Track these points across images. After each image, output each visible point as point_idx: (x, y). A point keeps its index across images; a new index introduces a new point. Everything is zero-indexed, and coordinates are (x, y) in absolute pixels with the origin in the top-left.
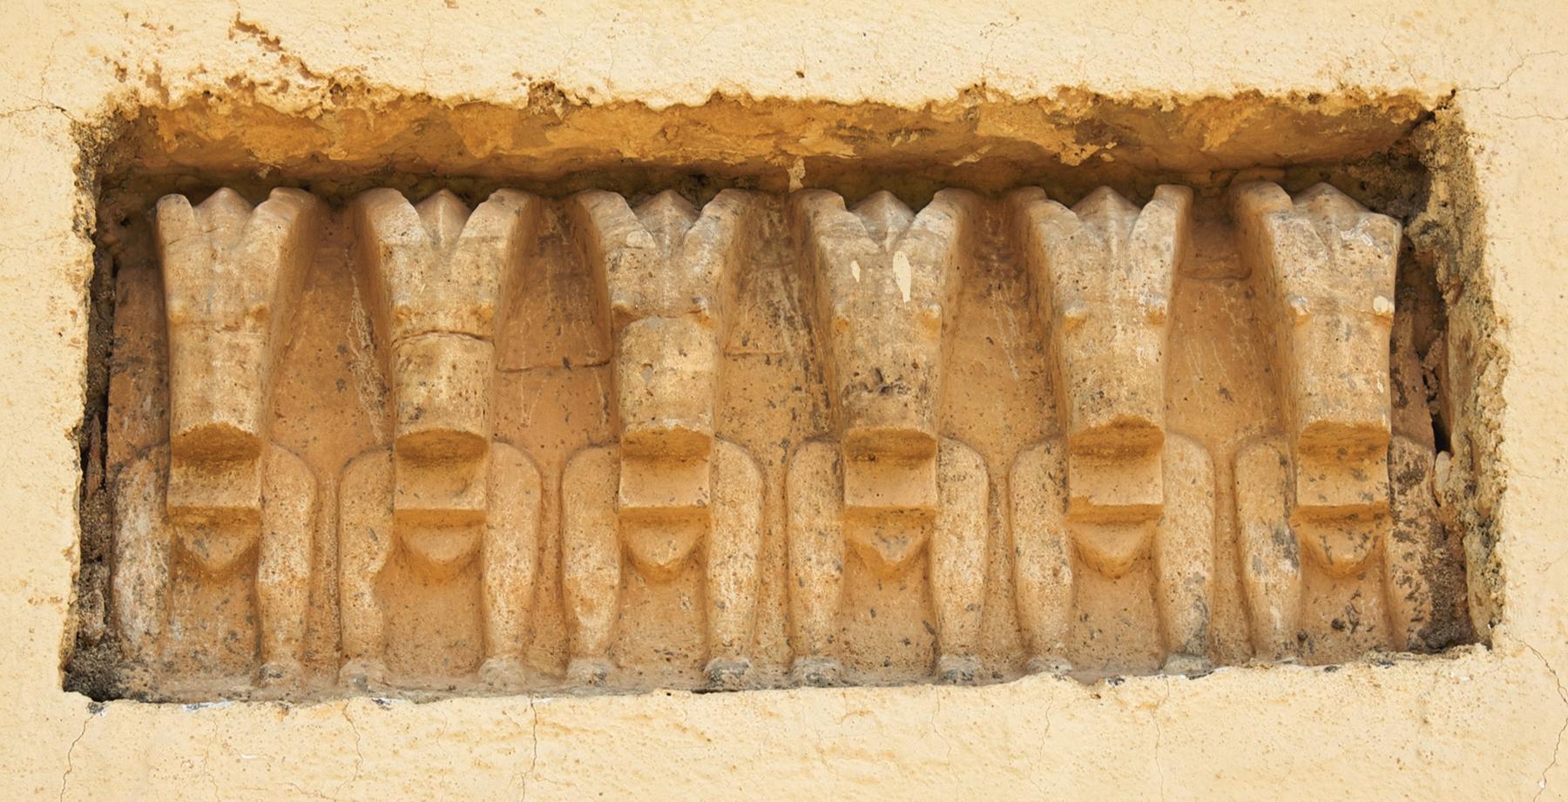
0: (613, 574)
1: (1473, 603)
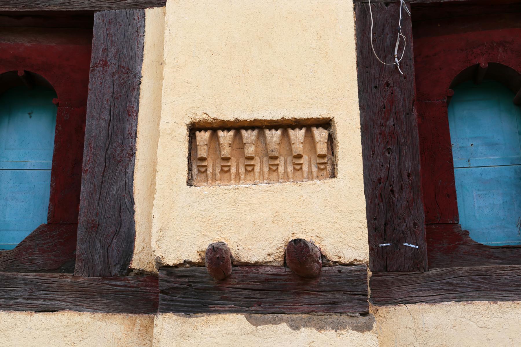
0: (244, 171)
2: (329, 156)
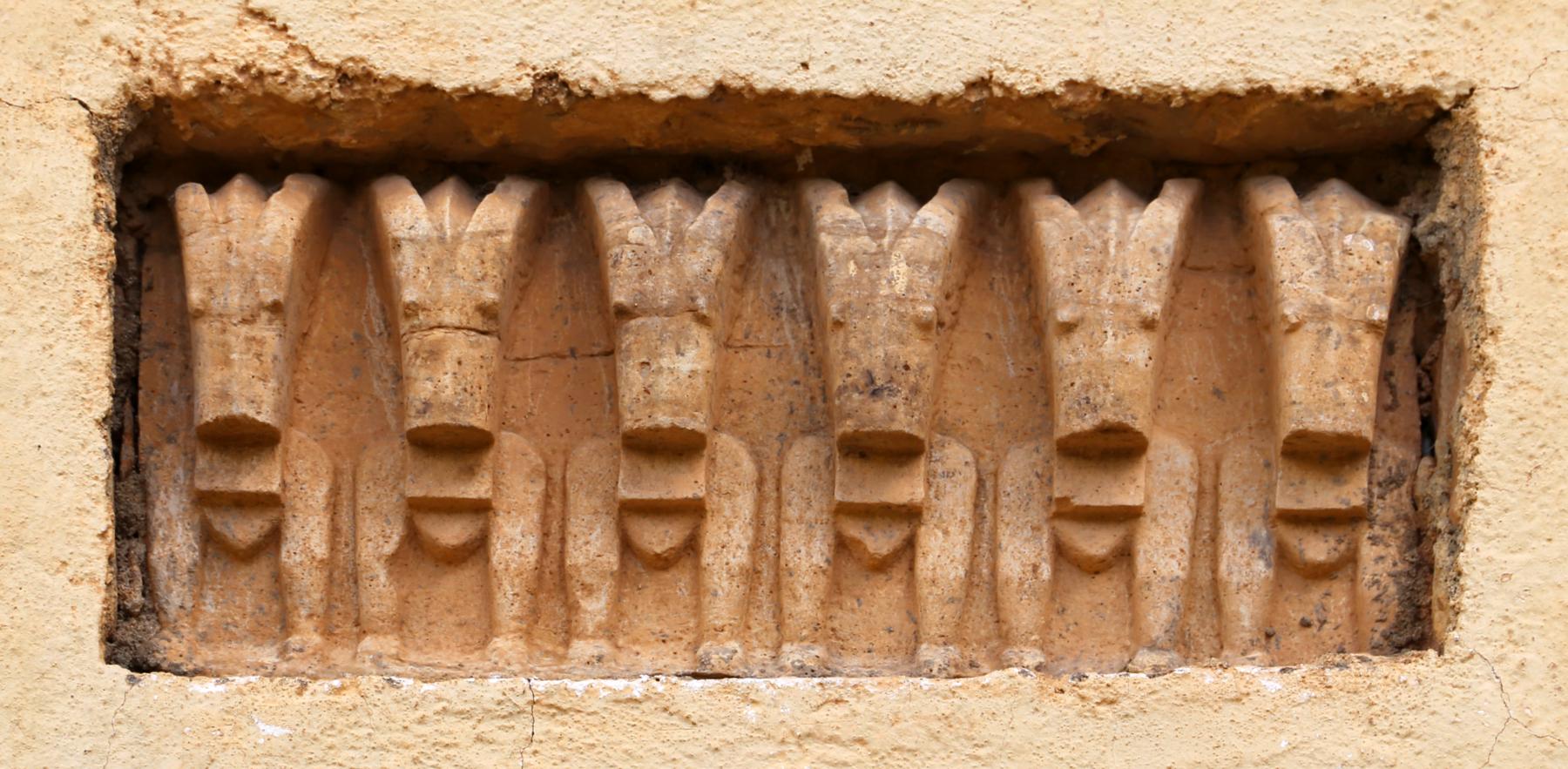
0: (612, 560)
1: (1435, 607)
2: (1392, 453)
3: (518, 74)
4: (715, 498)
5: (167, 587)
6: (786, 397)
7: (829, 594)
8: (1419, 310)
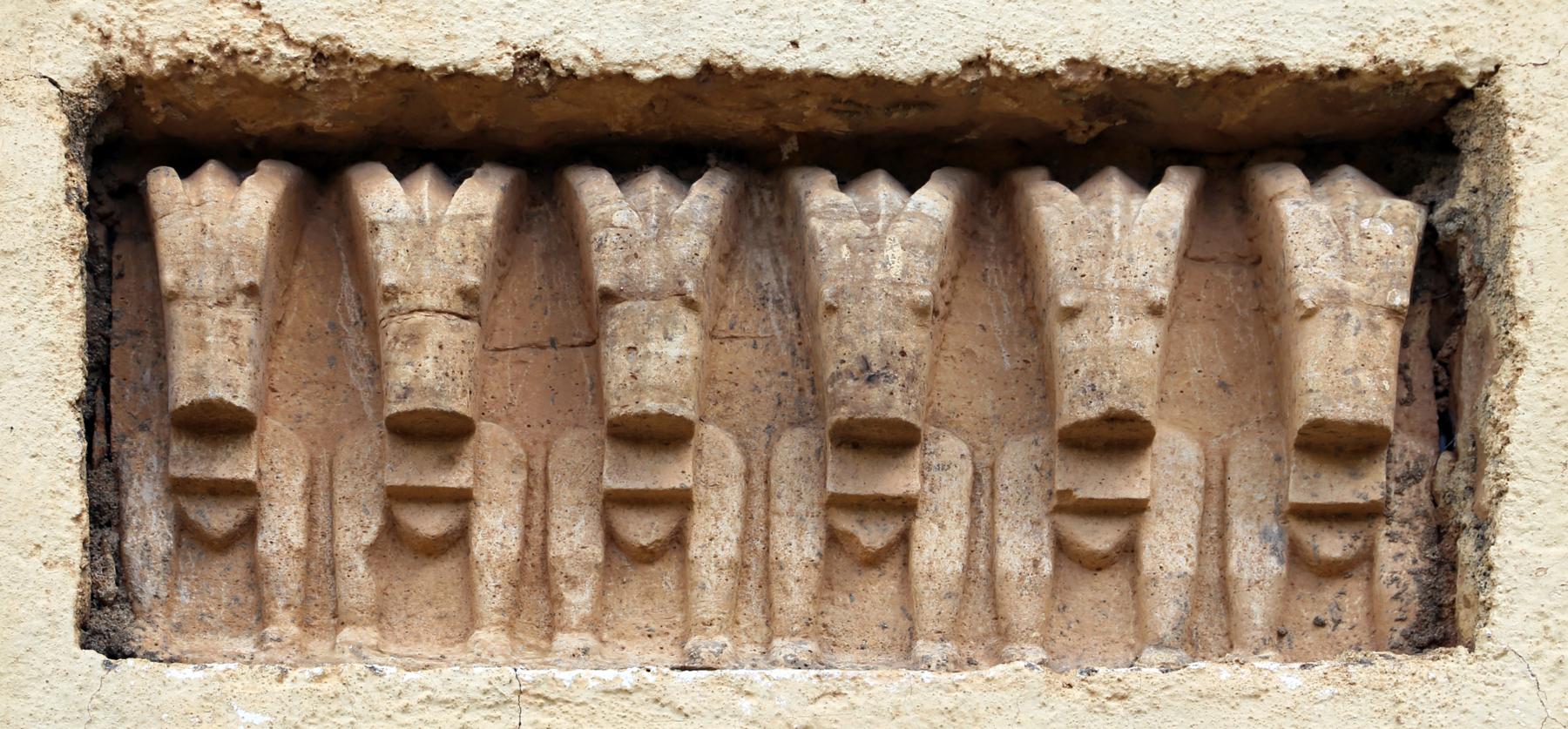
0: (596, 552)
1: (1460, 605)
2: (1410, 447)
3: (499, 53)
4: (702, 490)
5: (141, 576)
6: (773, 389)
7: (820, 589)
8: (1434, 302)
